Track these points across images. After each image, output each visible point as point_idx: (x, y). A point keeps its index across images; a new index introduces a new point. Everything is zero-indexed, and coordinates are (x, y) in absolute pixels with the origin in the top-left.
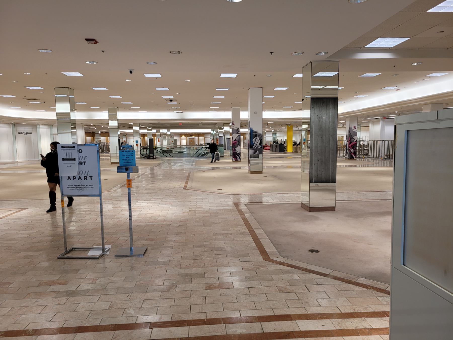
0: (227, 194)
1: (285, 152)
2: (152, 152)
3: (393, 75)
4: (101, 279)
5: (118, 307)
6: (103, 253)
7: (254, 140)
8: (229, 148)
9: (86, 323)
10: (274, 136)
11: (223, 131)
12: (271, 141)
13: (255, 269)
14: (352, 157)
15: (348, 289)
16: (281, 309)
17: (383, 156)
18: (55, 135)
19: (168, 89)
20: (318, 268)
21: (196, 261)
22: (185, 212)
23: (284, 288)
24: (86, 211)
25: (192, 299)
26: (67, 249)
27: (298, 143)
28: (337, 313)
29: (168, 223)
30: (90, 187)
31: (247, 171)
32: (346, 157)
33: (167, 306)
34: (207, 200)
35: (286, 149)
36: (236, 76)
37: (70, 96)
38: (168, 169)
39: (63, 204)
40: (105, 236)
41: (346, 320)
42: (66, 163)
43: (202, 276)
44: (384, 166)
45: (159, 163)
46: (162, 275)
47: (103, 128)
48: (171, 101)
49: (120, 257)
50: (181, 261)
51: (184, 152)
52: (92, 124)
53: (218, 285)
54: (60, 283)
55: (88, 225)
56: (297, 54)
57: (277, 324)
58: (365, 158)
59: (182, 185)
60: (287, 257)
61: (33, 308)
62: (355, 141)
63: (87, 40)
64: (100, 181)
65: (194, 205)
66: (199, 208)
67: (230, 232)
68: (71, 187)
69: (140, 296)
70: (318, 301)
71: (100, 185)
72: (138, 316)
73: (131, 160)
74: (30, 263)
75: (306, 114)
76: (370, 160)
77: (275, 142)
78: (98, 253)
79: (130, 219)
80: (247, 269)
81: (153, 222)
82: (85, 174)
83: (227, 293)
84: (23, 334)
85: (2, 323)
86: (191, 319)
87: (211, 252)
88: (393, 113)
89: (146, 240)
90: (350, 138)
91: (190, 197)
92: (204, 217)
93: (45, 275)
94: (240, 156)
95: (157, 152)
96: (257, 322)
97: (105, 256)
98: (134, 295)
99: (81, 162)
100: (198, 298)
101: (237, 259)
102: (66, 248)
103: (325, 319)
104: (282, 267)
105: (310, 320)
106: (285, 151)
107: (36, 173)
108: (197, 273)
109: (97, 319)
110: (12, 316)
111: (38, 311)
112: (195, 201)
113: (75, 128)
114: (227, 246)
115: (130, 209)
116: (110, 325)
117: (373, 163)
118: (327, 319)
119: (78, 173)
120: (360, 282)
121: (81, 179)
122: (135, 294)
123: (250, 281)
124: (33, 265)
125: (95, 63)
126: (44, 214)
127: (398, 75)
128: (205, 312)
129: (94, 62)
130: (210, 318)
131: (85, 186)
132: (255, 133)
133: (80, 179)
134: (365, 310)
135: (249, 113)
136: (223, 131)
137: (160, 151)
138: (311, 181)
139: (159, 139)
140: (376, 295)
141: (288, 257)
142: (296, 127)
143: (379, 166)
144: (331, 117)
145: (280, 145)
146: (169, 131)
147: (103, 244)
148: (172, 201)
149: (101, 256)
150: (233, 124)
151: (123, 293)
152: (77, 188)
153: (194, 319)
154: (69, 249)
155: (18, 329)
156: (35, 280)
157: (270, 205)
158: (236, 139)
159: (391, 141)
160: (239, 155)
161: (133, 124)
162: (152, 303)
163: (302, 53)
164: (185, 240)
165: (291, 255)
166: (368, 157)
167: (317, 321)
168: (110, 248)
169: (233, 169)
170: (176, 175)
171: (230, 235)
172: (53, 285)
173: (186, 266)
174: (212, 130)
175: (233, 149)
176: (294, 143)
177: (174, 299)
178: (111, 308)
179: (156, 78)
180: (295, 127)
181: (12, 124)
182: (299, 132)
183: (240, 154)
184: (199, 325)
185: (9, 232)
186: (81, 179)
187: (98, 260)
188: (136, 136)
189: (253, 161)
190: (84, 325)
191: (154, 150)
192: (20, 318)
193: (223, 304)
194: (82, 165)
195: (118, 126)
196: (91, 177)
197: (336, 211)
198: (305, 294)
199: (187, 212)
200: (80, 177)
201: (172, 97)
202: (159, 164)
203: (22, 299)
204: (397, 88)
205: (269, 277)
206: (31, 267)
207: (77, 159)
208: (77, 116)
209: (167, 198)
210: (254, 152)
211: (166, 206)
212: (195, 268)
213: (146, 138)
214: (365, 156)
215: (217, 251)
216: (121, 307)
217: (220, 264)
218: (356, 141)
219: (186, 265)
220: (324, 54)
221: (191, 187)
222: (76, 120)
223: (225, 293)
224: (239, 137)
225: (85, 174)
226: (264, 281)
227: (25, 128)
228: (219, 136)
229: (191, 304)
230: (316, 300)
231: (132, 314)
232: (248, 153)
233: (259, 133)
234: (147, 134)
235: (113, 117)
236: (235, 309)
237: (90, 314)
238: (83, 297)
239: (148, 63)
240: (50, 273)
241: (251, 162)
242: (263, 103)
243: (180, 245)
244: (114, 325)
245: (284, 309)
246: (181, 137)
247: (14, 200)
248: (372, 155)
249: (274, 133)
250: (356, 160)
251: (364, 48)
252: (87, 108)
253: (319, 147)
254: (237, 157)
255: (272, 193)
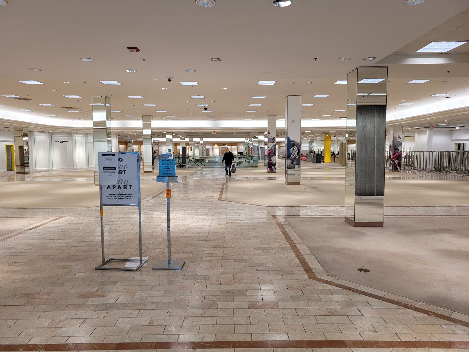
0: (265, 205)
1: (323, 162)
2: (184, 161)
3: (443, 82)
4: (140, 292)
5: (159, 323)
6: (141, 265)
7: (291, 149)
8: (395, 158)
9: (126, 340)
10: (311, 146)
11: (257, 140)
12: (307, 151)
13: (301, 288)
14: (397, 169)
15: (406, 314)
16: (333, 334)
17: (431, 168)
18: (90, 143)
19: (203, 97)
20: (370, 289)
21: (237, 277)
22: (221, 224)
23: (334, 311)
24: (121, 221)
25: (236, 319)
26: (104, 259)
27: (336, 153)
28: (396, 341)
29: (205, 235)
30: (129, 196)
31: (284, 182)
32: (389, 168)
33: (209, 325)
34: (243, 212)
35: (323, 159)
36: (274, 83)
37: (107, 105)
38: (200, 178)
39: (102, 214)
40: (143, 248)
41: (407, 349)
42: (106, 172)
43: (244, 293)
44: (432, 179)
45: (192, 173)
46: (202, 291)
47: (136, 137)
48: (206, 109)
49: (158, 270)
50: (221, 277)
51: (217, 161)
52: (126, 133)
53: (262, 304)
54: (98, 296)
55: (124, 235)
56: (343, 60)
57: (330, 350)
58: (410, 170)
59: (217, 195)
60: (334, 276)
61: (73, 320)
62: (400, 151)
63: (129, 48)
64: (139, 189)
65: (230, 216)
66: (236, 220)
67: (271, 246)
68: (110, 196)
69: (180, 313)
70: (374, 327)
71: (139, 195)
72: (179, 335)
73: (170, 169)
74: (68, 273)
75: (351, 123)
76: (416, 172)
77: (311, 152)
78: (135, 265)
79: (169, 230)
80: (292, 288)
81: (189, 233)
82: (124, 183)
83: (272, 313)
84: (64, 349)
85: (42, 336)
86: (236, 340)
87: (252, 267)
88: (443, 122)
89: (184, 252)
90: (394, 148)
91: (226, 208)
92: (241, 230)
93: (83, 286)
94: (275, 166)
95: (190, 161)
96: (308, 347)
97: (143, 268)
98: (174, 311)
99: (121, 171)
100: (242, 317)
101: (280, 276)
102: (103, 258)
103: (383, 348)
104: (329, 287)
105: (367, 348)
106: (322, 161)
107: (70, 181)
108: (238, 290)
109: (138, 335)
110: (52, 328)
111: (78, 324)
112: (232, 213)
113: (110, 137)
114: (268, 262)
115: (169, 220)
116: (151, 343)
117: (420, 175)
118: (386, 347)
119: (118, 182)
120: (419, 307)
121: (121, 189)
122: (176, 310)
123: (297, 301)
124: (72, 275)
125: (135, 71)
126: (80, 223)
127: (449, 81)
128: (250, 334)
129: (134, 70)
130: (256, 340)
131: (124, 196)
132: (292, 143)
133: (109, 188)
134: (429, 339)
135: (287, 121)
136: (257, 140)
137: (192, 160)
138: (356, 194)
139: (191, 148)
140: (439, 323)
141: (336, 275)
142: (334, 137)
143: (426, 179)
144: (375, 126)
145: (316, 155)
146: (201, 140)
147: (141, 256)
148: (208, 212)
149: (139, 268)
150: (269, 133)
151: (162, 308)
152: (116, 197)
153: (239, 340)
154: (106, 260)
155: (58, 342)
156: (73, 291)
157: (311, 218)
158: (272, 149)
159: (439, 152)
160: (274, 165)
161: (167, 132)
162: (193, 321)
163: (348, 59)
164: (224, 254)
165: (338, 274)
166: (414, 169)
167: (375, 350)
168: (147, 260)
169: (268, 179)
170: (210, 185)
171: (271, 250)
172: (92, 297)
173: (227, 281)
174: (245, 139)
175: (268, 159)
176: (332, 153)
177: (216, 318)
178: (151, 325)
179: (192, 86)
180: (333, 136)
181: (49, 132)
182: (337, 142)
183: (276, 164)
184: (244, 348)
185: (47, 241)
186: (121, 189)
187: (135, 272)
188: (169, 145)
189: (290, 172)
190: (125, 341)
191: (187, 159)
192: (60, 330)
193: (268, 325)
194: (122, 174)
195: (152, 134)
196: (130, 186)
197: (384, 227)
198: (359, 318)
199: (224, 224)
200: (119, 186)
201: (207, 105)
202: (192, 174)
203: (62, 311)
204: (448, 95)
205: (317, 298)
206: (70, 277)
207: (117, 168)
208: (113, 124)
209: (202, 209)
210: (291, 162)
211: (202, 218)
212: (236, 284)
213: (178, 147)
214: (410, 168)
215: (258, 267)
216: (161, 324)
217: (263, 281)
218: (401, 152)
219: (226, 281)
220: (372, 59)
221: (226, 198)
222: (112, 129)
223: (270, 313)
224: (274, 146)
225: (124, 183)
226: (312, 302)
227: (61, 136)
228: (253, 146)
229: (234, 323)
230: (372, 325)
231: (173, 332)
232: (285, 163)
233: (297, 143)
234: (180, 143)
235: (147, 126)
236: (283, 331)
237: (131, 330)
238: (123, 311)
239: (187, 71)
240: (88, 284)
241: (288, 172)
242: (301, 111)
243: (219, 259)
244: (155, 342)
245: (337, 334)
246: (214, 146)
247: (62, 207)
248: (419, 167)
249: (311, 143)
250: (400, 172)
251: (415, 53)
252: (121, 117)
253: (362, 157)
254: (273, 167)
255: (312, 206)
